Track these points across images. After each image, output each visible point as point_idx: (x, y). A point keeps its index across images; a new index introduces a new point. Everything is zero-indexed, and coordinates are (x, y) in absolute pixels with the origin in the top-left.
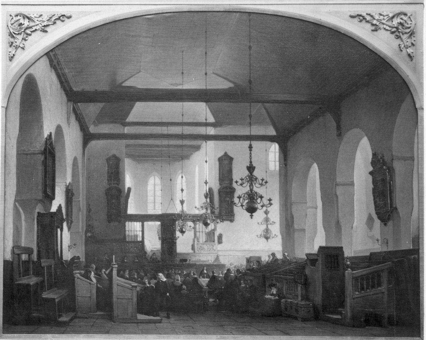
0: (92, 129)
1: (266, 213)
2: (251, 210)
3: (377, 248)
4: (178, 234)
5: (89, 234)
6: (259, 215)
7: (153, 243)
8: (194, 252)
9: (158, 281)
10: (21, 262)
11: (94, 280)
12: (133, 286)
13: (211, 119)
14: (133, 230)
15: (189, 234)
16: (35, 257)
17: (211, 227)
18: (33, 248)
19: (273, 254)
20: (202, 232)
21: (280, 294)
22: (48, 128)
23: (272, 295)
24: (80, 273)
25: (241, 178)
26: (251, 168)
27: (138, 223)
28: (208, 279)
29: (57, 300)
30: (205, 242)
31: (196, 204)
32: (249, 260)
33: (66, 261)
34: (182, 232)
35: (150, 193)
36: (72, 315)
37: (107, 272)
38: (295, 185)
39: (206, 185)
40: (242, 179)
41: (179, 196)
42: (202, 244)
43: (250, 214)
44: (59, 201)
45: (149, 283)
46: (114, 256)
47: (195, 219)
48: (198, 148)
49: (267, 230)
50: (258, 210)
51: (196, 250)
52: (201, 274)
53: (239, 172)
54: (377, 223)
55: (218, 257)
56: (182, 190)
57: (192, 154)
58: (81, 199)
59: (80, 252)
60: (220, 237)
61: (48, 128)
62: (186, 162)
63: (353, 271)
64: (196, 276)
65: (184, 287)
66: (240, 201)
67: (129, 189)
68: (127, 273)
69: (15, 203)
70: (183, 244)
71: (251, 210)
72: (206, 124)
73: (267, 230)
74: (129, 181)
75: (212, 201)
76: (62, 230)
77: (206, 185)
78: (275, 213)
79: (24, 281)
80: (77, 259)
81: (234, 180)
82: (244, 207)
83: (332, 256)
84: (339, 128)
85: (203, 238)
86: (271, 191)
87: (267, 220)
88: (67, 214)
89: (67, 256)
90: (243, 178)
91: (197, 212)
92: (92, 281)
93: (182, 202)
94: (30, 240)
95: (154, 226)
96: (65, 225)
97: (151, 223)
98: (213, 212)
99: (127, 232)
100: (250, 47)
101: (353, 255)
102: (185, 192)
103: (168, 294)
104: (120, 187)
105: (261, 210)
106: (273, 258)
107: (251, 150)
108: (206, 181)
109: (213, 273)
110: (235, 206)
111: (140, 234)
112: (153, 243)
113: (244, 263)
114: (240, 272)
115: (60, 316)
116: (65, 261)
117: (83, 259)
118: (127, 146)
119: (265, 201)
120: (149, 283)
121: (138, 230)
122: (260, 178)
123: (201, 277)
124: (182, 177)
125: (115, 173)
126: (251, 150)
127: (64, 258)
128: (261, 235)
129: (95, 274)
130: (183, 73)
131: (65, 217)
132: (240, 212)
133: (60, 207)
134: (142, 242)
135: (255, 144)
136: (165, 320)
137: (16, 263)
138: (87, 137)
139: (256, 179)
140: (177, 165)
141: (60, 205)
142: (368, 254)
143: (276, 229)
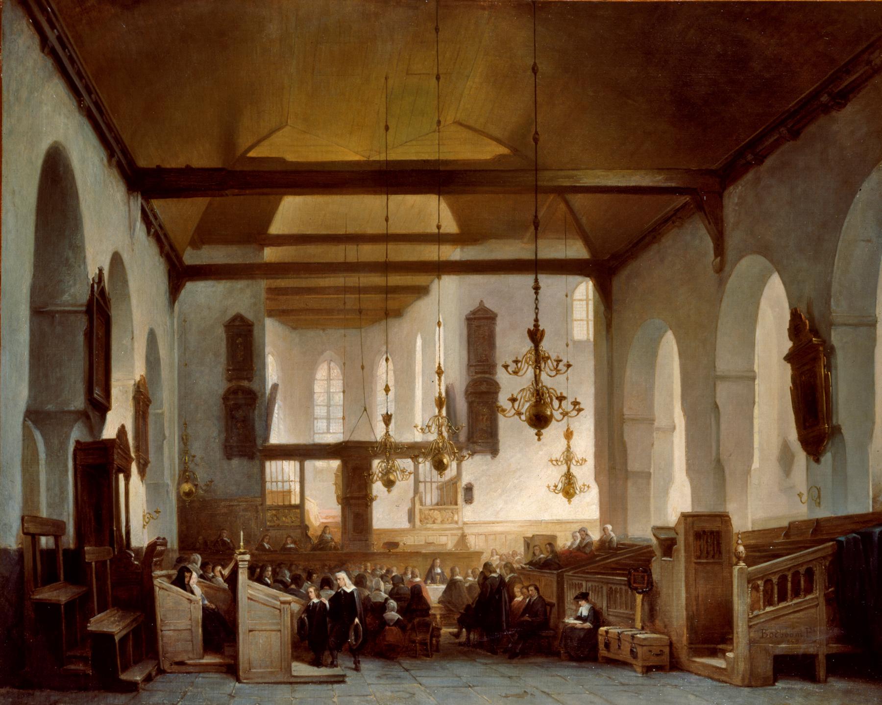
0: (190, 257)
1: (569, 435)
3: (802, 512)
4: (378, 488)
5: (186, 487)
7: (322, 508)
8: (414, 526)
9: (338, 594)
10: (38, 554)
11: (198, 590)
12: (283, 603)
13: (450, 226)
14: (280, 478)
15: (404, 486)
16: (69, 539)
17: (451, 472)
18: (65, 520)
19: (583, 532)
20: (431, 482)
21: (596, 617)
22: (96, 258)
23: (579, 618)
24: (169, 577)
25: (514, 359)
26: (536, 335)
27: (292, 462)
28: (444, 587)
29: (117, 638)
30: (437, 504)
31: (419, 423)
32: (528, 543)
33: (138, 551)
34: (389, 484)
35: (320, 398)
36: (149, 668)
37: (226, 572)
38: (631, 375)
39: (440, 378)
40: (516, 362)
41: (381, 404)
42: (431, 510)
43: (536, 431)
44: (118, 419)
45: (318, 596)
46: (242, 533)
47: (414, 451)
48: (422, 291)
49: (569, 477)
50: (554, 422)
51: (418, 523)
52: (430, 576)
53: (511, 344)
54: (801, 457)
55: (463, 537)
56: (387, 389)
57: (408, 305)
58: (166, 401)
59: (169, 529)
60: (469, 489)
61: (96, 258)
62: (394, 324)
63: (749, 566)
64: (418, 579)
65: (393, 603)
66: (513, 406)
67: (275, 387)
68: (269, 571)
69: (24, 420)
70: (388, 512)
71: (539, 420)
72: (440, 239)
73: (569, 477)
74: (273, 371)
75: (451, 416)
76: (127, 478)
77: (440, 378)
78: (585, 443)
79: (47, 594)
80: (161, 545)
81: (500, 363)
82: (523, 417)
83: (707, 535)
84: (720, 249)
85: (431, 497)
86: (580, 385)
87: (568, 457)
88: (137, 449)
89: (140, 538)
90: (520, 358)
91: (418, 437)
92: (192, 592)
93: (387, 419)
94: (60, 502)
95: (325, 474)
96: (134, 468)
97: (320, 464)
98: (454, 435)
99: (268, 485)
100: (535, 70)
101: (749, 527)
102: (391, 394)
103: (357, 620)
104: (255, 386)
105: (560, 423)
106: (583, 539)
107: (537, 293)
108: (439, 367)
109: (452, 571)
110: (505, 416)
111: (296, 487)
112: (322, 508)
113: (521, 549)
114: (512, 570)
115: (125, 668)
116: (134, 551)
117: (173, 542)
118: (270, 290)
119: (567, 405)
120: (317, 597)
121: (292, 478)
122: (553, 356)
123: (429, 582)
124: (387, 360)
125: (242, 344)
126: (537, 293)
127: (135, 543)
128: (556, 486)
129: (201, 576)
130: (387, 128)
131: (133, 455)
132: (511, 427)
133: (122, 431)
134: (301, 507)
135: (546, 280)
136: (351, 676)
137: (28, 557)
138: (179, 275)
139: (548, 358)
140: (374, 334)
141: (123, 427)
142: (785, 524)
143: (585, 474)
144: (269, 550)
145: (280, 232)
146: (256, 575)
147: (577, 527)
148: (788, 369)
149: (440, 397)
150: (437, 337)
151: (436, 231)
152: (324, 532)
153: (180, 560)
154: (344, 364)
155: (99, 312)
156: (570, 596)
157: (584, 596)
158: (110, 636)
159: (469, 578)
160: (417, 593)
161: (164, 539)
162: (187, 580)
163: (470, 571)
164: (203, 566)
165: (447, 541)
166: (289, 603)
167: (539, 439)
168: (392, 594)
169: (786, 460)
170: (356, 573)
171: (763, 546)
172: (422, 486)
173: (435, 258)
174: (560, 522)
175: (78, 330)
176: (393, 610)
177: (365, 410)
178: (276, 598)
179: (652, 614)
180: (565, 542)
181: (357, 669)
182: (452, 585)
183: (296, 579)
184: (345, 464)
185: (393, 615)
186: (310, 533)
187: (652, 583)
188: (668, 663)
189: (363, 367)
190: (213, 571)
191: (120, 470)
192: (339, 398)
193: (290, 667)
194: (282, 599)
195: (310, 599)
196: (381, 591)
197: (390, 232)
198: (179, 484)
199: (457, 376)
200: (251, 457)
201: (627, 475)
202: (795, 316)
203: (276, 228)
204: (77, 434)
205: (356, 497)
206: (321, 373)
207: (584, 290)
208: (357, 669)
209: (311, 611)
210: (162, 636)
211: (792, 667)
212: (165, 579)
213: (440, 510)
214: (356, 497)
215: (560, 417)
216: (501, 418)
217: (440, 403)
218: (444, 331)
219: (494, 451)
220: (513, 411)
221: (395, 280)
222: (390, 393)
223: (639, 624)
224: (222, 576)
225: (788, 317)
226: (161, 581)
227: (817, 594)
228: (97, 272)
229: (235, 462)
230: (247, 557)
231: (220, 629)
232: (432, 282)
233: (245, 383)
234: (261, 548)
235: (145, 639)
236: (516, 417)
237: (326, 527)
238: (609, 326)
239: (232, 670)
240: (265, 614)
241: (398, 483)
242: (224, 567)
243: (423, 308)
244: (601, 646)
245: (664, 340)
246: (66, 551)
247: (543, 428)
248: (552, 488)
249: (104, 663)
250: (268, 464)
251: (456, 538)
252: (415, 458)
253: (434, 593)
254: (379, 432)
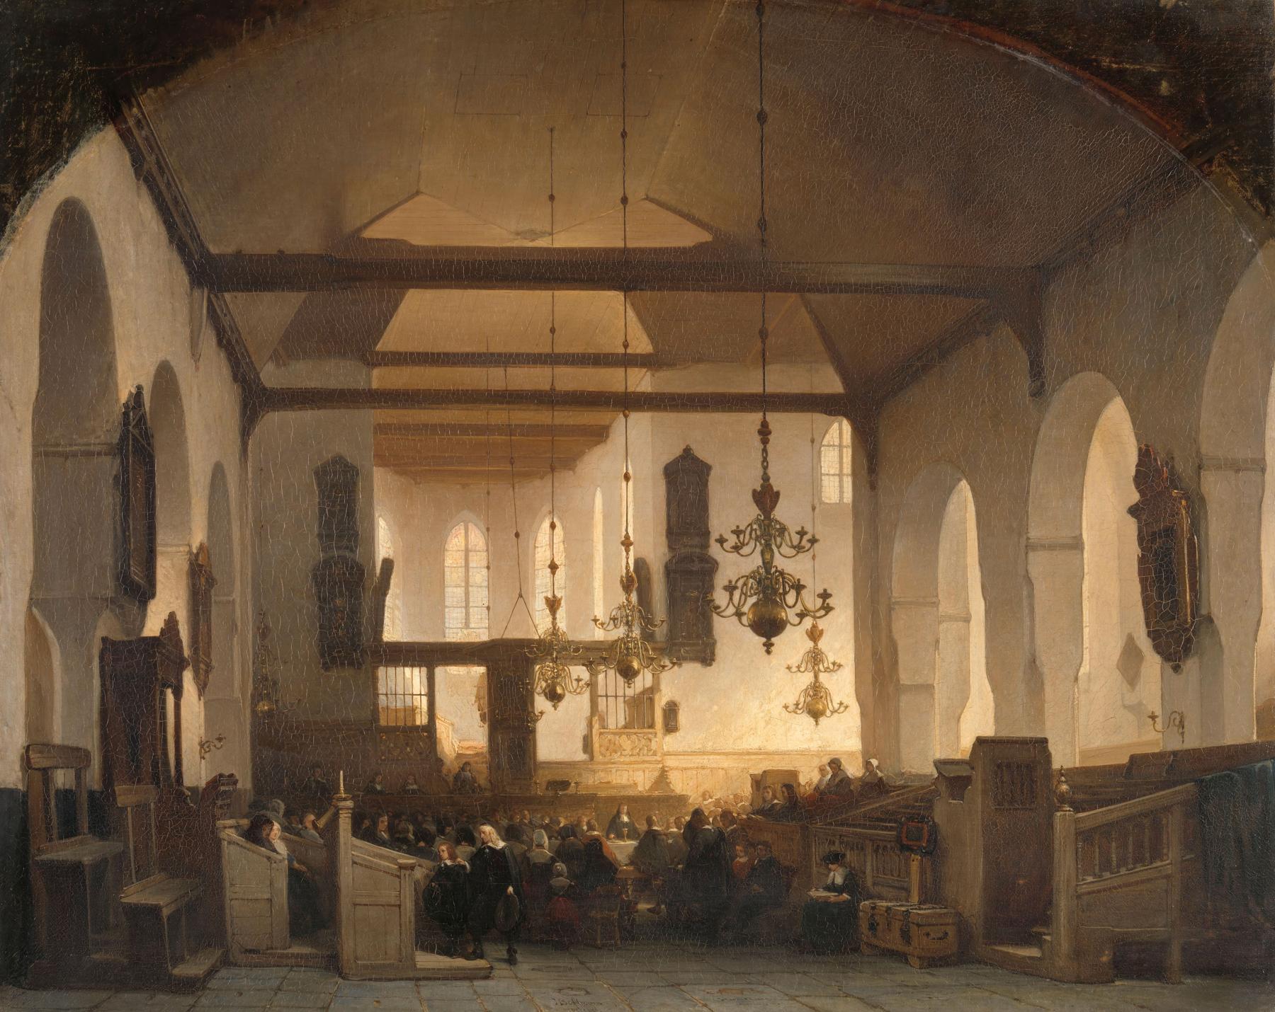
0: (271, 375)
1: (814, 635)
2: (768, 627)
3: (1152, 740)
4: (541, 703)
5: (264, 707)
6: (793, 642)
7: (461, 730)
8: (592, 758)
11: (281, 847)
12: (401, 867)
13: (642, 344)
17: (644, 680)
19: (835, 764)
21: (853, 884)
22: (131, 372)
23: (832, 888)
24: (237, 827)
26: (766, 497)
29: (166, 912)
30: (625, 727)
31: (596, 610)
32: (759, 783)
33: (194, 790)
34: (554, 697)
35: (453, 575)
36: (214, 956)
37: (321, 823)
40: (737, 532)
43: (764, 640)
44: (168, 604)
47: (594, 655)
48: (600, 435)
49: (816, 691)
51: (596, 753)
52: (614, 826)
53: (729, 510)
54: (1153, 663)
55: (663, 774)
56: (553, 567)
59: (238, 763)
60: (671, 711)
61: (131, 372)
65: (560, 866)
68: (384, 822)
70: (558, 733)
71: (768, 627)
72: (628, 361)
73: (816, 691)
74: (385, 540)
76: (178, 693)
77: (627, 551)
78: (840, 637)
81: (714, 535)
83: (1012, 764)
84: (1036, 371)
85: (617, 715)
86: (829, 568)
87: (815, 658)
89: (196, 772)
90: (742, 528)
93: (553, 604)
94: (76, 724)
96: (188, 676)
98: (648, 636)
102: (560, 573)
103: (511, 889)
107: (765, 442)
108: (627, 537)
109: (650, 822)
112: (461, 730)
113: (747, 790)
114: (733, 821)
115: (177, 960)
116: (188, 789)
117: (245, 783)
120: (451, 855)
121: (416, 691)
122: (793, 528)
124: (553, 526)
127: (189, 780)
132: (733, 635)
133: (171, 622)
134: (430, 728)
136: (502, 970)
138: (255, 401)
143: (842, 686)
145: (228, 873)
146: (364, 829)
147: (826, 760)
148: (1132, 526)
149: (629, 577)
151: (622, 350)
152: (463, 769)
153: (254, 805)
154: (488, 530)
155: (139, 446)
156: (817, 852)
157: (836, 858)
158: (155, 911)
159: (670, 827)
160: (595, 848)
161: (232, 775)
162: (264, 834)
163: (672, 820)
164: (288, 813)
165: (640, 780)
166: (412, 868)
167: (768, 652)
169: (1130, 659)
170: (505, 822)
171: (1097, 785)
172: (602, 702)
173: (620, 388)
174: (802, 753)
175: (111, 471)
176: (560, 875)
177: (521, 596)
178: (394, 860)
179: (932, 894)
180: (810, 777)
182: (650, 839)
183: (423, 835)
184: (491, 674)
185: (561, 882)
186: (444, 771)
187: (935, 841)
190: (301, 822)
192: (479, 576)
193: (413, 959)
194: (400, 861)
195: (441, 859)
197: (557, 351)
199: (653, 548)
200: (356, 664)
201: (899, 689)
202: (1145, 455)
203: (389, 342)
204: (106, 626)
205: (509, 714)
207: (840, 432)
208: (511, 961)
211: (1135, 962)
212: (232, 830)
213: (628, 735)
214: (509, 714)
215: (797, 620)
217: (627, 585)
218: (635, 487)
219: (706, 657)
220: (731, 610)
221: (566, 417)
223: (915, 899)
225: (1133, 459)
226: (229, 830)
227: (1172, 859)
229: (334, 673)
231: (312, 902)
232: (613, 420)
233: (347, 554)
234: (370, 790)
235: (204, 919)
236: (735, 618)
240: (379, 879)
241: (568, 697)
242: (319, 816)
243: (602, 463)
245: (954, 498)
246: (91, 794)
247: (775, 635)
249: (148, 952)
250: (381, 671)
251: (656, 774)
252: (589, 665)
253: (621, 849)
254: (540, 625)
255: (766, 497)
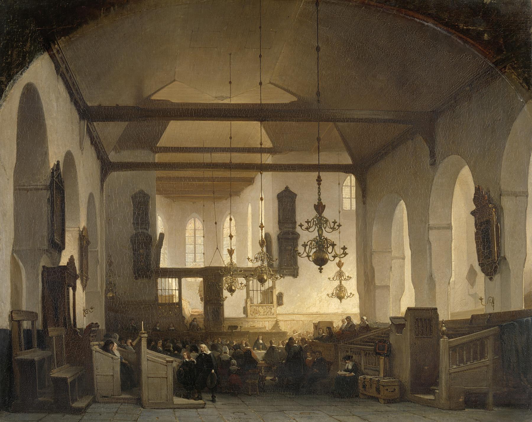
0: (113, 157)
1: (340, 265)
2: (321, 262)
3: (481, 309)
4: (226, 293)
5: (110, 295)
6: (331, 268)
7: (192, 304)
8: (247, 316)
11: (117, 353)
12: (168, 362)
13: (268, 144)
17: (269, 284)
19: (348, 318)
21: (356, 369)
22: (55, 155)
23: (347, 370)
26: (320, 207)
29: (69, 380)
31: (249, 255)
32: (316, 326)
33: (81, 329)
34: (231, 291)
35: (189, 240)
37: (134, 343)
40: (308, 222)
41: (226, 244)
43: (319, 267)
44: (70, 252)
47: (248, 273)
48: (250, 181)
49: (340, 288)
52: (256, 345)
53: (304, 213)
54: (481, 277)
55: (277, 323)
56: (231, 237)
57: (243, 189)
59: (99, 318)
60: (280, 297)
61: (55, 155)
65: (234, 361)
67: (162, 235)
68: (160, 343)
70: (233, 306)
71: (321, 262)
72: (262, 151)
73: (340, 288)
74: (161, 225)
76: (74, 289)
77: (262, 230)
78: (350, 266)
81: (298, 223)
83: (422, 319)
84: (432, 155)
85: (257, 298)
86: (346, 237)
87: (340, 274)
89: (82, 322)
93: (231, 252)
96: (78, 282)
98: (270, 265)
103: (213, 371)
104: (150, 232)
106: (348, 324)
107: (319, 184)
108: (262, 224)
109: (271, 343)
112: (192, 304)
113: (312, 329)
114: (306, 342)
115: (74, 401)
116: (79, 329)
117: (102, 327)
120: (189, 356)
121: (174, 288)
122: (331, 220)
124: (231, 219)
127: (78, 326)
129: (119, 346)
132: (306, 265)
133: (72, 259)
134: (180, 304)
136: (209, 404)
138: (106, 167)
141: (72, 257)
143: (351, 286)
144: (159, 330)
146: (152, 346)
148: (472, 219)
150: (261, 210)
153: (106, 336)
154: (204, 221)
155: (58, 186)
157: (349, 358)
158: (65, 380)
159: (280, 345)
160: (248, 353)
161: (97, 323)
164: (120, 339)
165: (267, 325)
166: (172, 362)
167: (321, 272)
168: (234, 356)
169: (471, 275)
170: (211, 343)
171: (458, 327)
172: (251, 293)
174: (335, 314)
175: (47, 196)
176: (234, 365)
177: (217, 248)
178: (164, 359)
179: (389, 373)
180: (338, 324)
181: (213, 401)
182: (271, 350)
184: (205, 281)
185: (234, 368)
188: (400, 397)
189: (260, 27)
191: (69, 286)
196: (227, 353)
198: (106, 294)
199: (273, 229)
200: (149, 277)
201: (375, 287)
202: (478, 190)
203: (162, 142)
205: (213, 298)
206: (190, 226)
207: (350, 180)
208: (213, 401)
209: (185, 364)
210: (97, 378)
211: (473, 401)
213: (262, 306)
214: (213, 298)
216: (299, 259)
217: (262, 244)
218: (265, 203)
219: (295, 274)
220: (305, 254)
222: (233, 238)
224: (132, 345)
225: (473, 191)
226: (96, 346)
228: (56, 163)
229: (139, 281)
230: (146, 335)
231: (130, 376)
234: (154, 330)
235: (85, 384)
237: (195, 318)
238: (364, 196)
239: (139, 402)
240: (159, 367)
243: (251, 193)
244: (361, 387)
245: (398, 208)
246: (38, 331)
248: (330, 295)
249: (62, 397)
250: (159, 280)
251: (274, 323)
253: (259, 354)
254: (226, 260)
255: (320, 207)
